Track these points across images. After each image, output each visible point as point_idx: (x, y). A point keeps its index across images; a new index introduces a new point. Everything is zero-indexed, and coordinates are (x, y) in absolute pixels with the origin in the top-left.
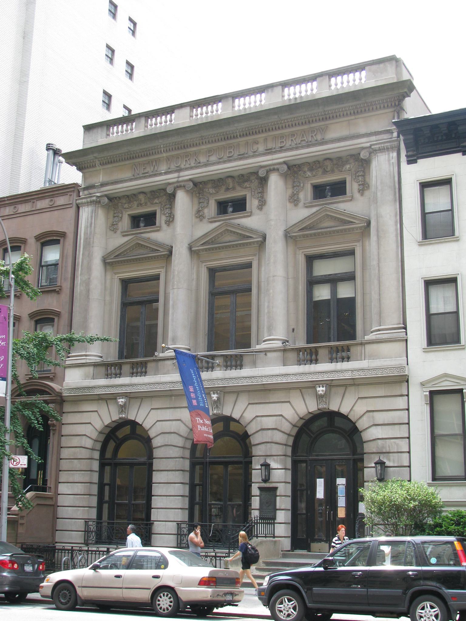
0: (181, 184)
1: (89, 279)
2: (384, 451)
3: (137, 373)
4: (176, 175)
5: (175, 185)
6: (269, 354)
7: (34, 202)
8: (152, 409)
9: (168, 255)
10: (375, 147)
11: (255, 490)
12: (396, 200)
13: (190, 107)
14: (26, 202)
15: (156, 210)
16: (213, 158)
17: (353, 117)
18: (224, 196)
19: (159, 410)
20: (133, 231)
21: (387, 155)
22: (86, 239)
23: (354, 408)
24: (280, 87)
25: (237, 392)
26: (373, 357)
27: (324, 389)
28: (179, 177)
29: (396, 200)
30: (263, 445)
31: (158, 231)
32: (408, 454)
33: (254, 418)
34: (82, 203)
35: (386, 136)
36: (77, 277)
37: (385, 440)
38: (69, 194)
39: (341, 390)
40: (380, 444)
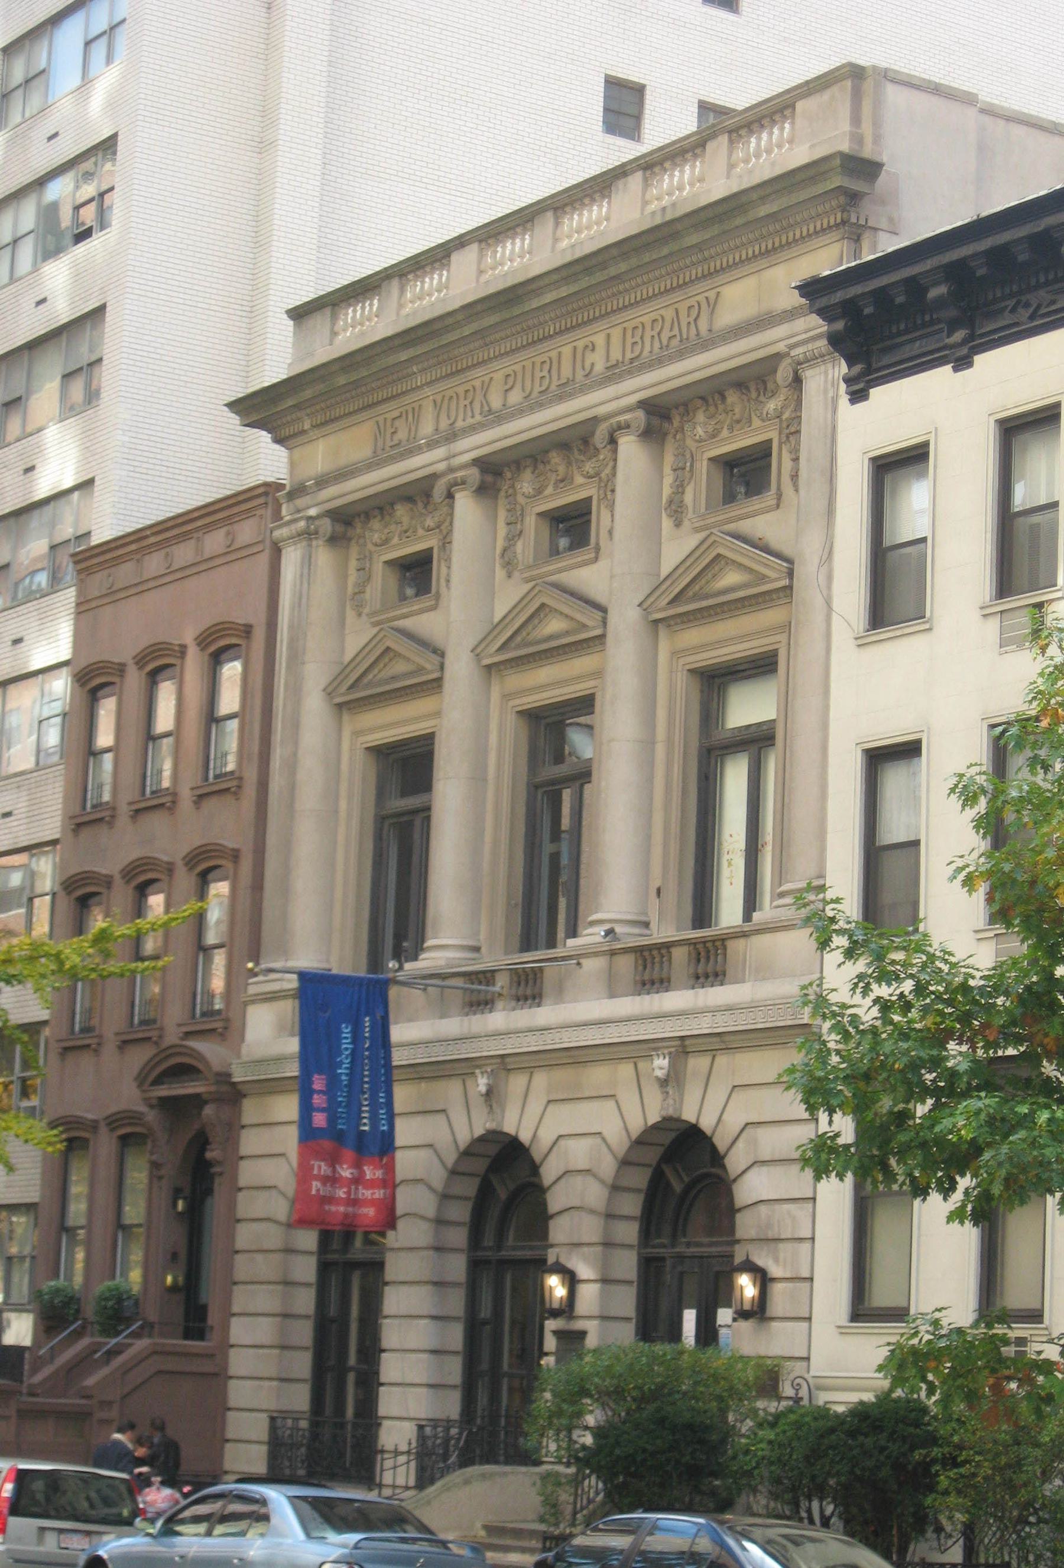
0: (618, 419)
3: (707, 976)
4: (440, 452)
7: (198, 539)
14: (185, 537)
22: (292, 641)
24: (550, 215)
27: (666, 1061)
38: (195, 535)
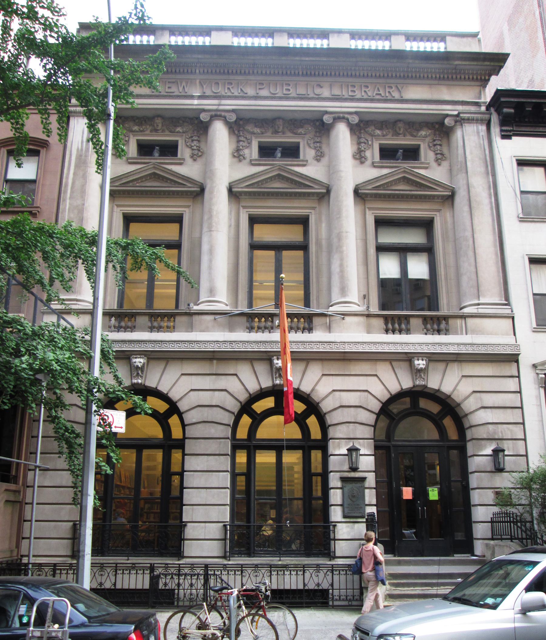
1: (84, 204)
2: (496, 437)
4: (215, 102)
5: (213, 113)
6: (347, 318)
8: (183, 374)
9: (198, 193)
10: (465, 115)
11: (334, 481)
12: (488, 173)
13: (233, 32)
15: (177, 141)
16: (264, 93)
17: (436, 82)
18: (270, 139)
19: (193, 377)
20: (141, 159)
21: (475, 127)
23: (458, 388)
25: (303, 358)
26: (475, 332)
28: (219, 105)
29: (488, 173)
30: (344, 426)
31: (181, 164)
32: (524, 442)
33: (330, 393)
34: (75, 112)
35: (473, 109)
36: (64, 200)
37: (497, 426)
39: (441, 366)
40: (490, 429)
